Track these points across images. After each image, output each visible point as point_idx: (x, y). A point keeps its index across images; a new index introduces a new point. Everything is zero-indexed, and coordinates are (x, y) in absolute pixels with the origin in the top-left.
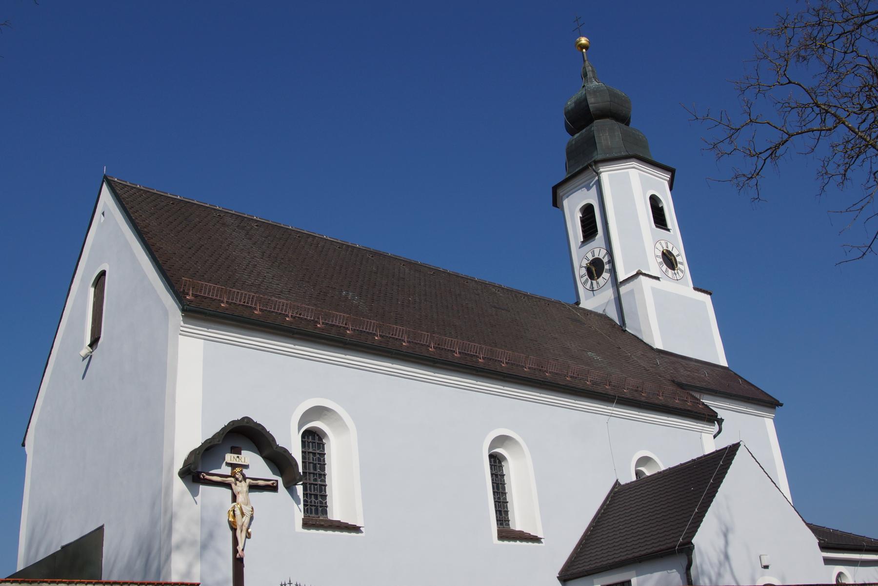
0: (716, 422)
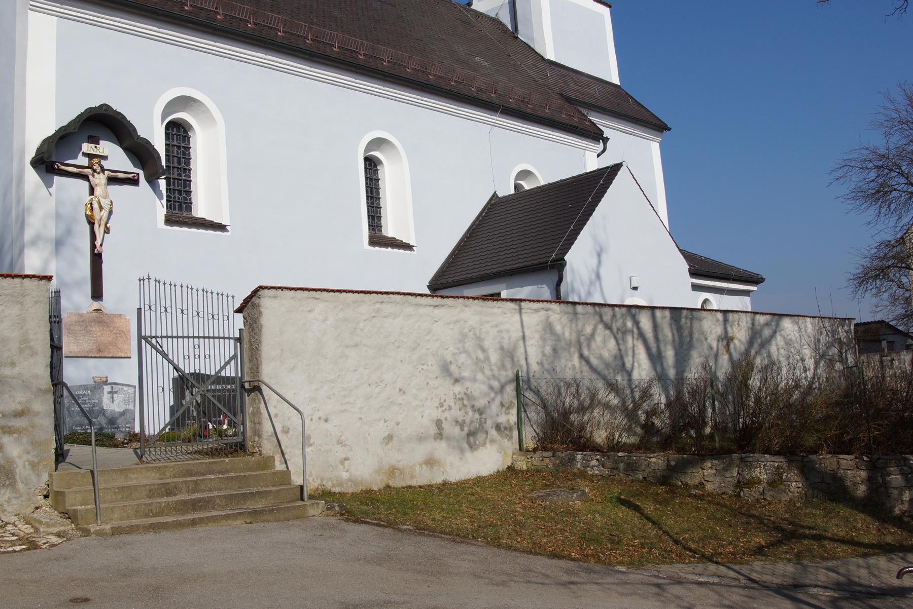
0: (601, 141)
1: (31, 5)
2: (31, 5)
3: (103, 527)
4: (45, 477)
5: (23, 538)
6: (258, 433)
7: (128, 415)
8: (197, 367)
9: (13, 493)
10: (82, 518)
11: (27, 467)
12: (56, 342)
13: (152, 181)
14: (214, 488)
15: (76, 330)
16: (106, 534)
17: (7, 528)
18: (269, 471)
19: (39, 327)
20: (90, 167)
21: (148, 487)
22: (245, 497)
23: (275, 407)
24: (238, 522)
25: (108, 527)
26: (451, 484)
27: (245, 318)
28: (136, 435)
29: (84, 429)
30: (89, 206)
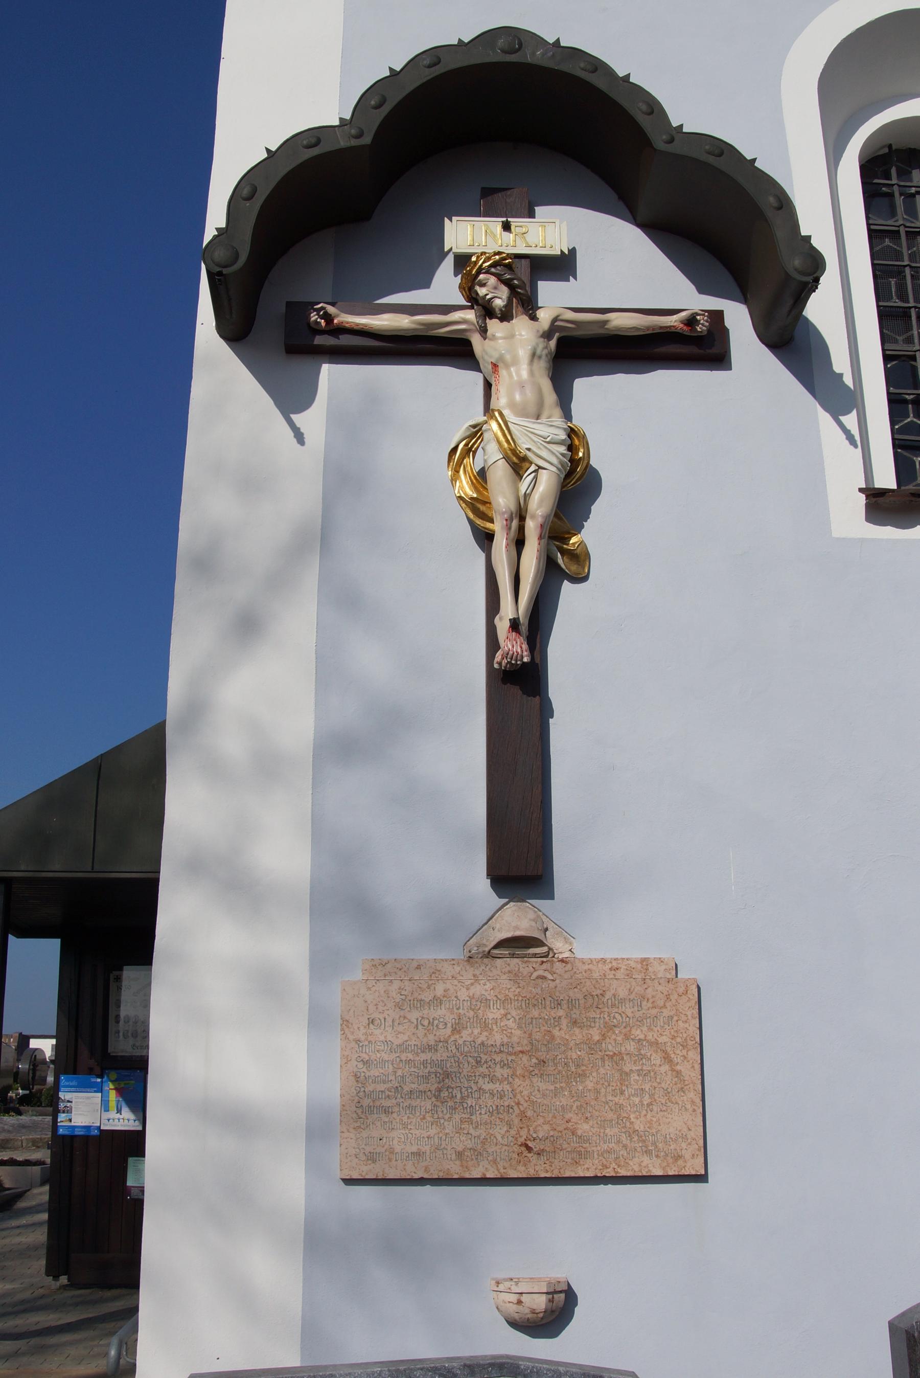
26: (813, 292)
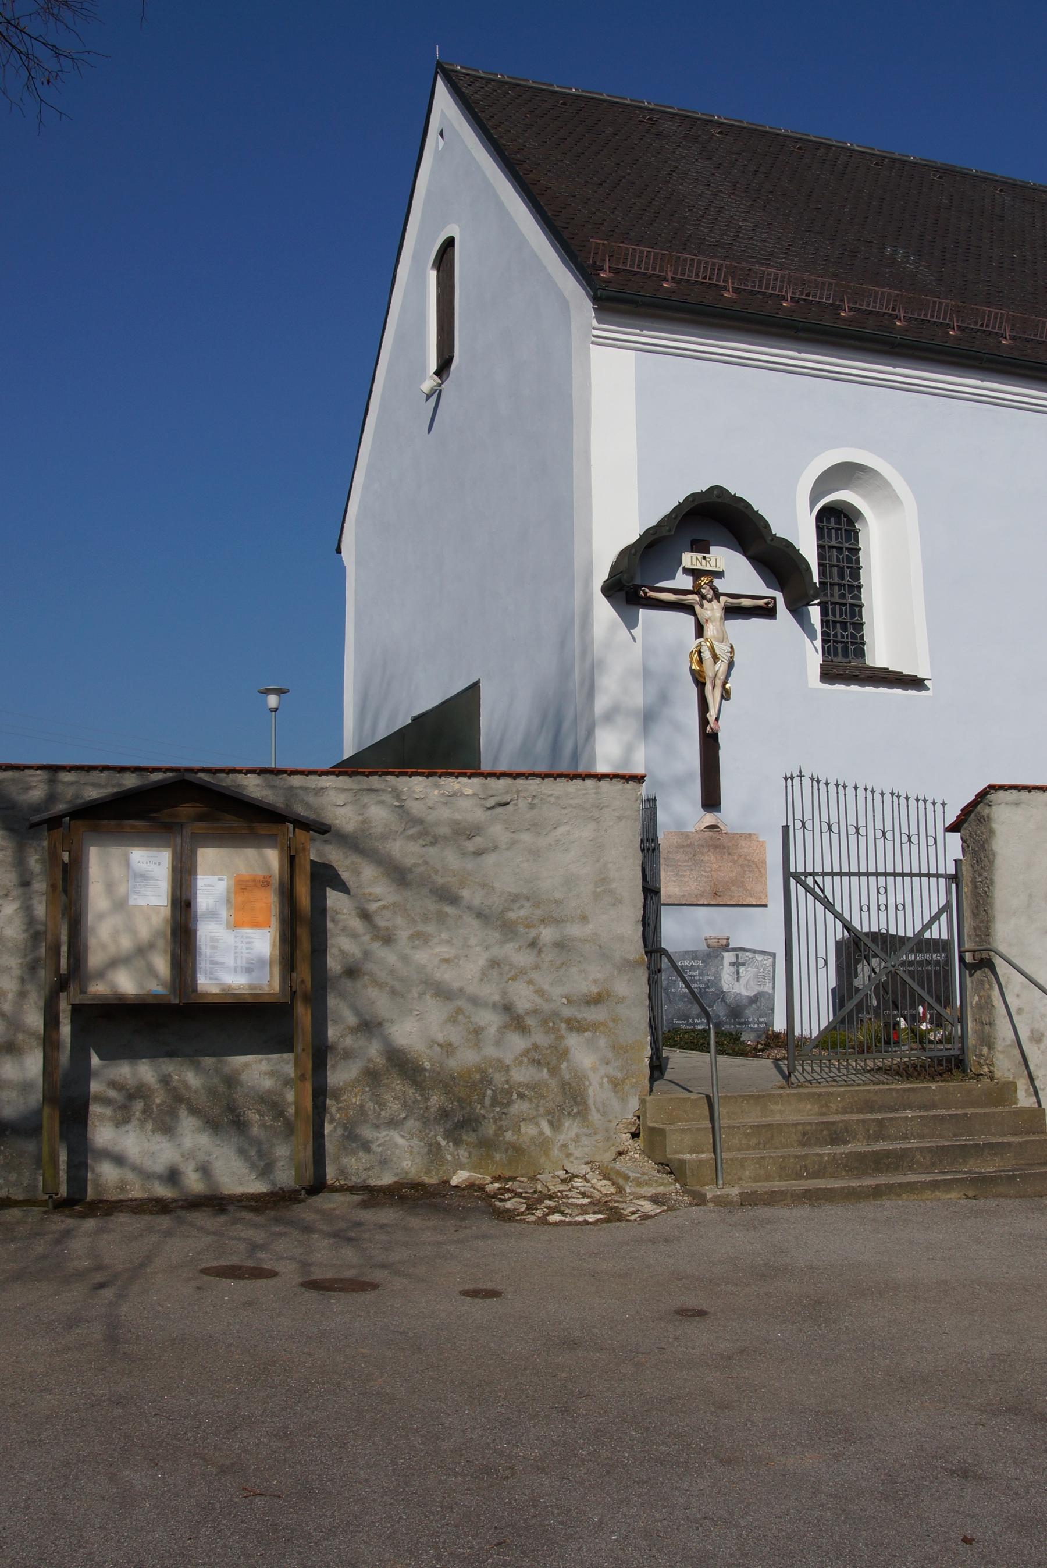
1: (594, 336)
2: (594, 336)
3: (726, 1191)
4: (634, 1104)
5: (599, 1201)
6: (987, 1041)
7: (763, 1002)
8: (883, 926)
9: (583, 1127)
10: (693, 1175)
11: (606, 1085)
12: (651, 883)
13: (797, 610)
14: (912, 1135)
15: (679, 861)
16: (731, 1203)
17: (574, 1184)
18: (1007, 1109)
19: (625, 858)
20: (698, 590)
21: (800, 1128)
22: (965, 1152)
23: (1018, 996)
24: (953, 1195)
25: (734, 1192)
27: (964, 841)
28: (776, 1036)
29: (691, 1024)
30: (696, 656)
